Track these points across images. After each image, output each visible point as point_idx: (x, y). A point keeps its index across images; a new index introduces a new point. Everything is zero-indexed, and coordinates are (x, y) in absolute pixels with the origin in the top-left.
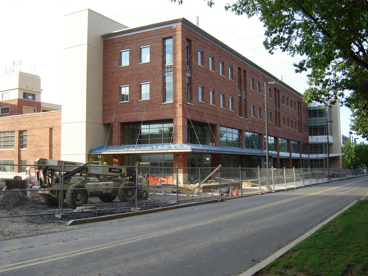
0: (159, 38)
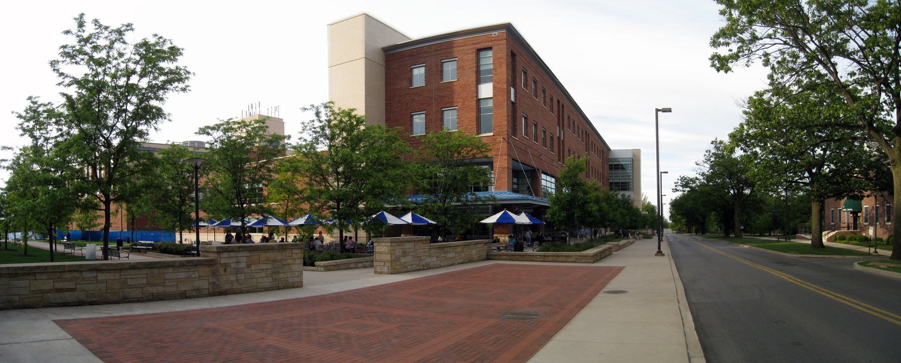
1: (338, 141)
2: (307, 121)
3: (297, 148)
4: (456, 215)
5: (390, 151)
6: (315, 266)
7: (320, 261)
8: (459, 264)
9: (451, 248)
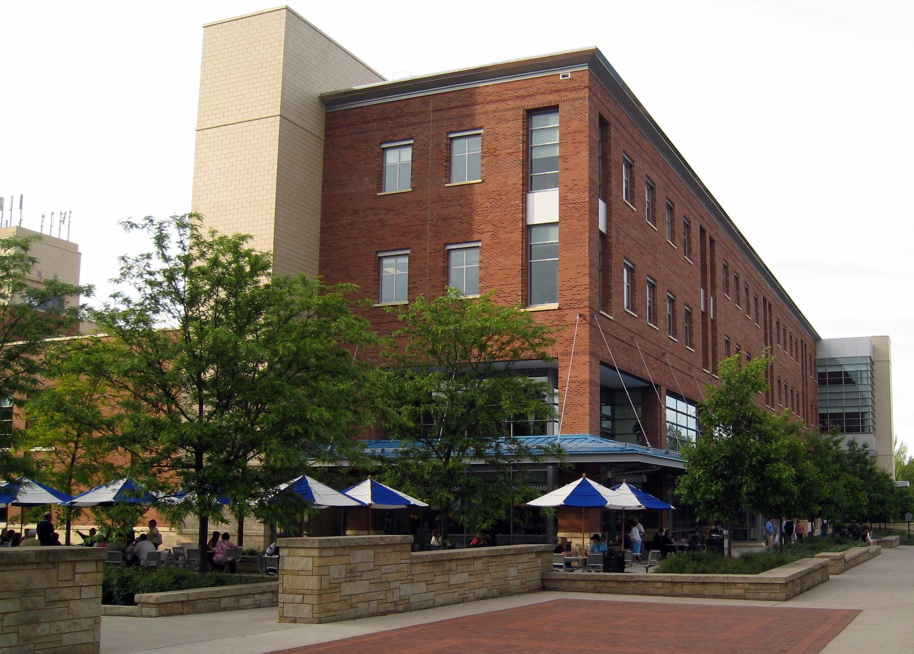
0: (513, 109)
1: (206, 310)
2: (133, 254)
3: (106, 319)
4: (473, 487)
5: (325, 338)
6: (136, 604)
7: (148, 592)
8: (478, 599)
9: (459, 563)
